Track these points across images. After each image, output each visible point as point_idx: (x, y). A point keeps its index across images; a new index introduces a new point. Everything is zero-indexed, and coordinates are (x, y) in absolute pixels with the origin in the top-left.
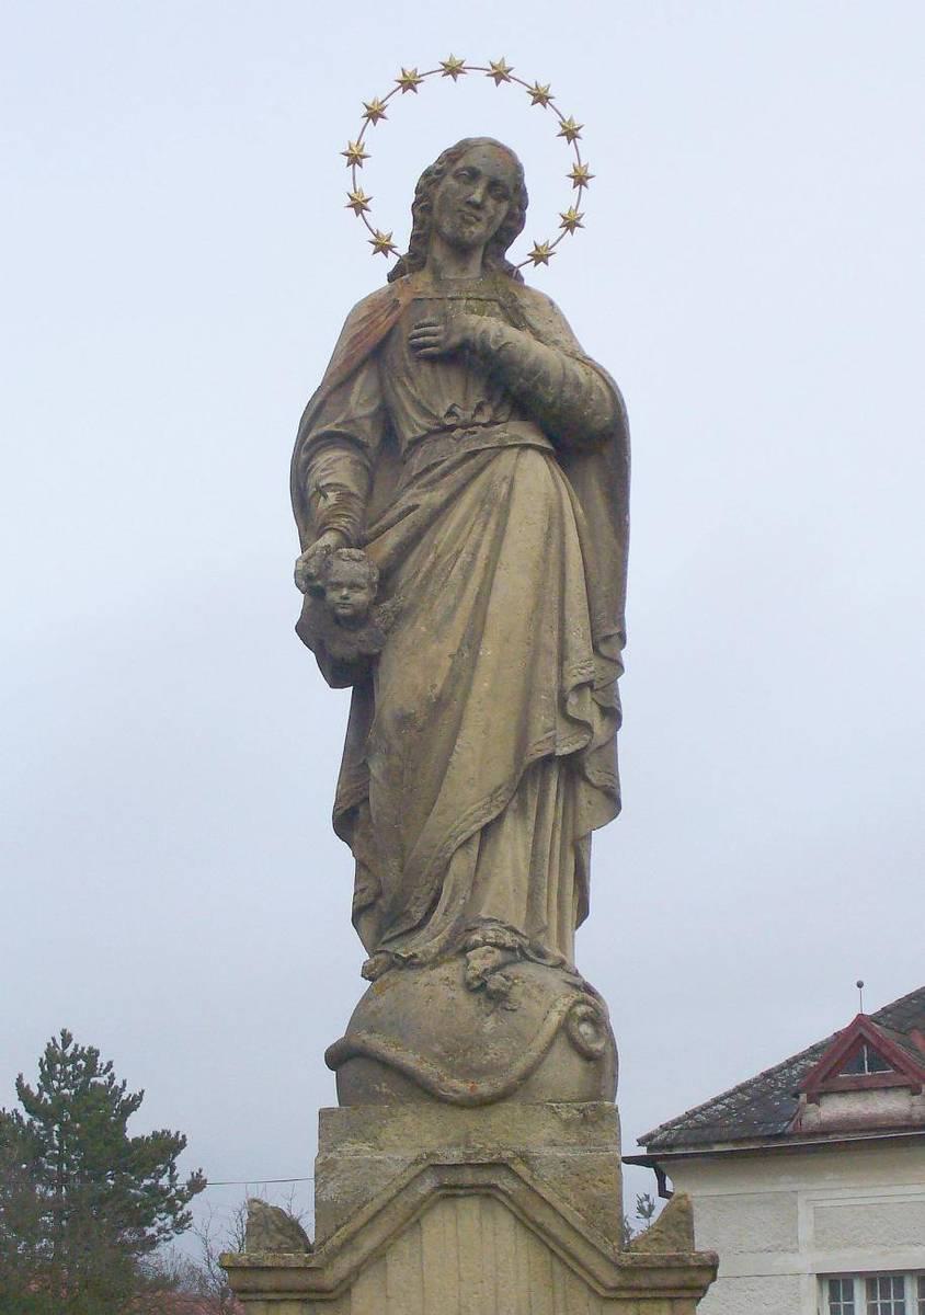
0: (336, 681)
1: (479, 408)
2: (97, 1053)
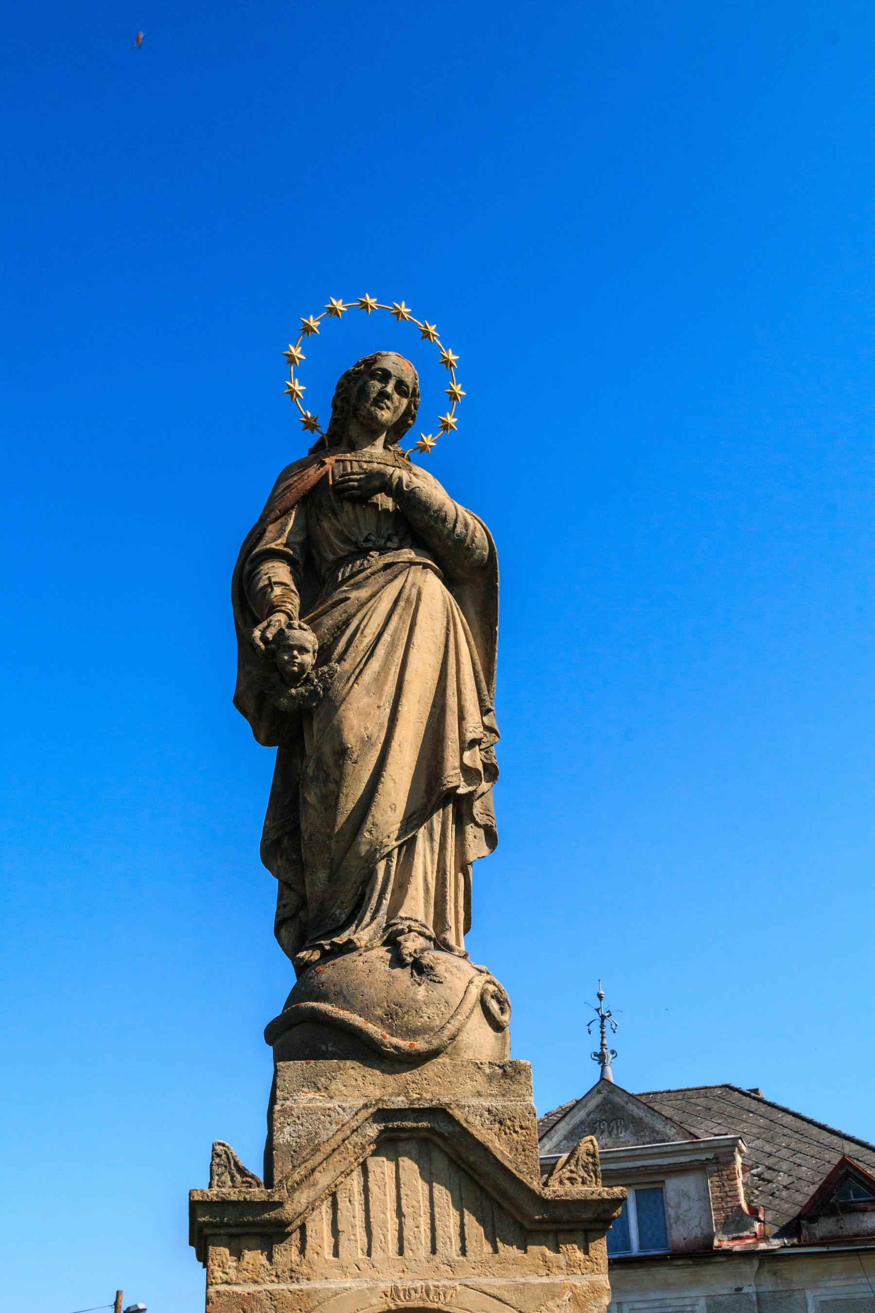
0: (267, 743)
1: (389, 539)
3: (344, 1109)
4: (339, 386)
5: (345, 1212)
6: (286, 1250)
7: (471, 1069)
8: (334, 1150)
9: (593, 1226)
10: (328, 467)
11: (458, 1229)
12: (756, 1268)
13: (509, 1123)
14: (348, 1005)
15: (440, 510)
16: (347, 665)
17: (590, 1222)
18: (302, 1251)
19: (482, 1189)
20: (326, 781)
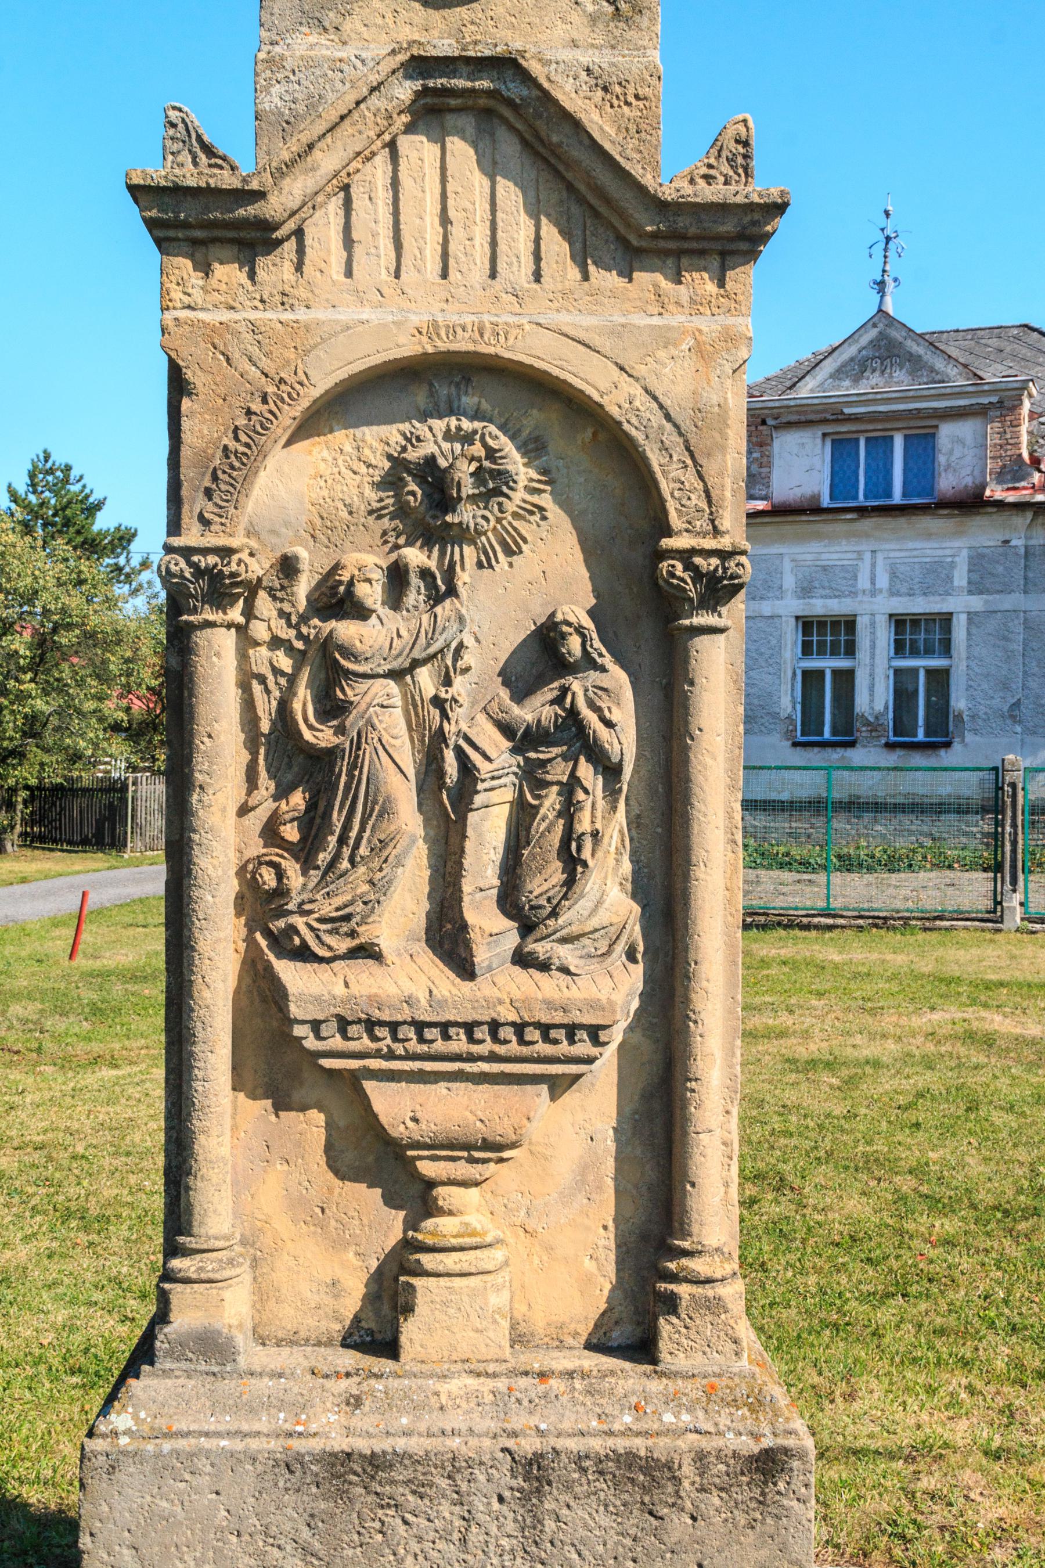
3: (363, 61)
5: (362, 214)
6: (275, 265)
8: (342, 118)
9: (733, 246)
11: (531, 246)
13: (618, 89)
18: (299, 267)
19: (570, 187)
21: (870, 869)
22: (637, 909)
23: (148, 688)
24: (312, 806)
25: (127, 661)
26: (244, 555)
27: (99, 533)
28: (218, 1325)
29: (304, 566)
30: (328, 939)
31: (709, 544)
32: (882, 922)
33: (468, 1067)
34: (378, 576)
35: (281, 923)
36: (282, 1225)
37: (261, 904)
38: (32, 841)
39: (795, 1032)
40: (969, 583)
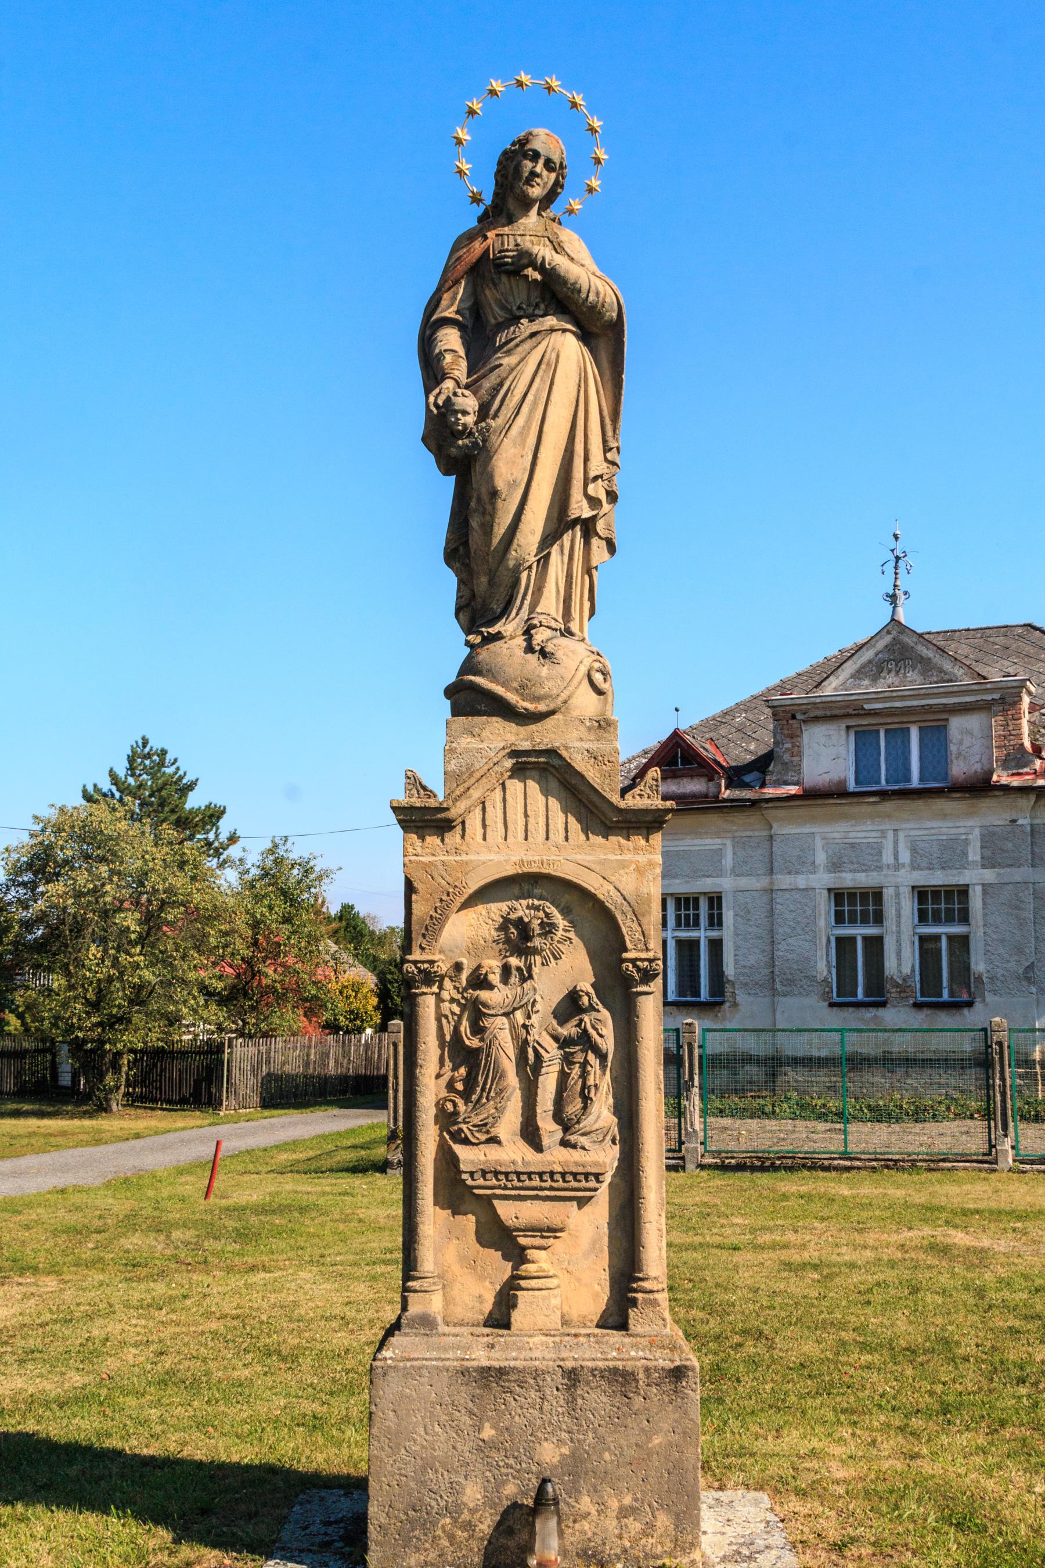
0: (447, 473)
1: (537, 306)
2: (166, 752)
4: (499, 163)
7: (577, 722)
10: (490, 241)
12: (1032, 802)
14: (495, 679)
15: (576, 283)
16: (500, 421)
17: (651, 822)
18: (463, 837)
20: (484, 514)
21: (898, 1120)
22: (616, 1120)
23: (243, 959)
24: (469, 1074)
25: (226, 934)
26: (440, 963)
27: (191, 811)
28: (429, 1312)
29: (465, 966)
30: (477, 1135)
31: (643, 955)
32: (892, 1164)
33: (540, 1193)
34: (498, 971)
35: (456, 1128)
36: (456, 1268)
37: (446, 1119)
38: (133, 1101)
39: (795, 1245)
40: (982, 858)
